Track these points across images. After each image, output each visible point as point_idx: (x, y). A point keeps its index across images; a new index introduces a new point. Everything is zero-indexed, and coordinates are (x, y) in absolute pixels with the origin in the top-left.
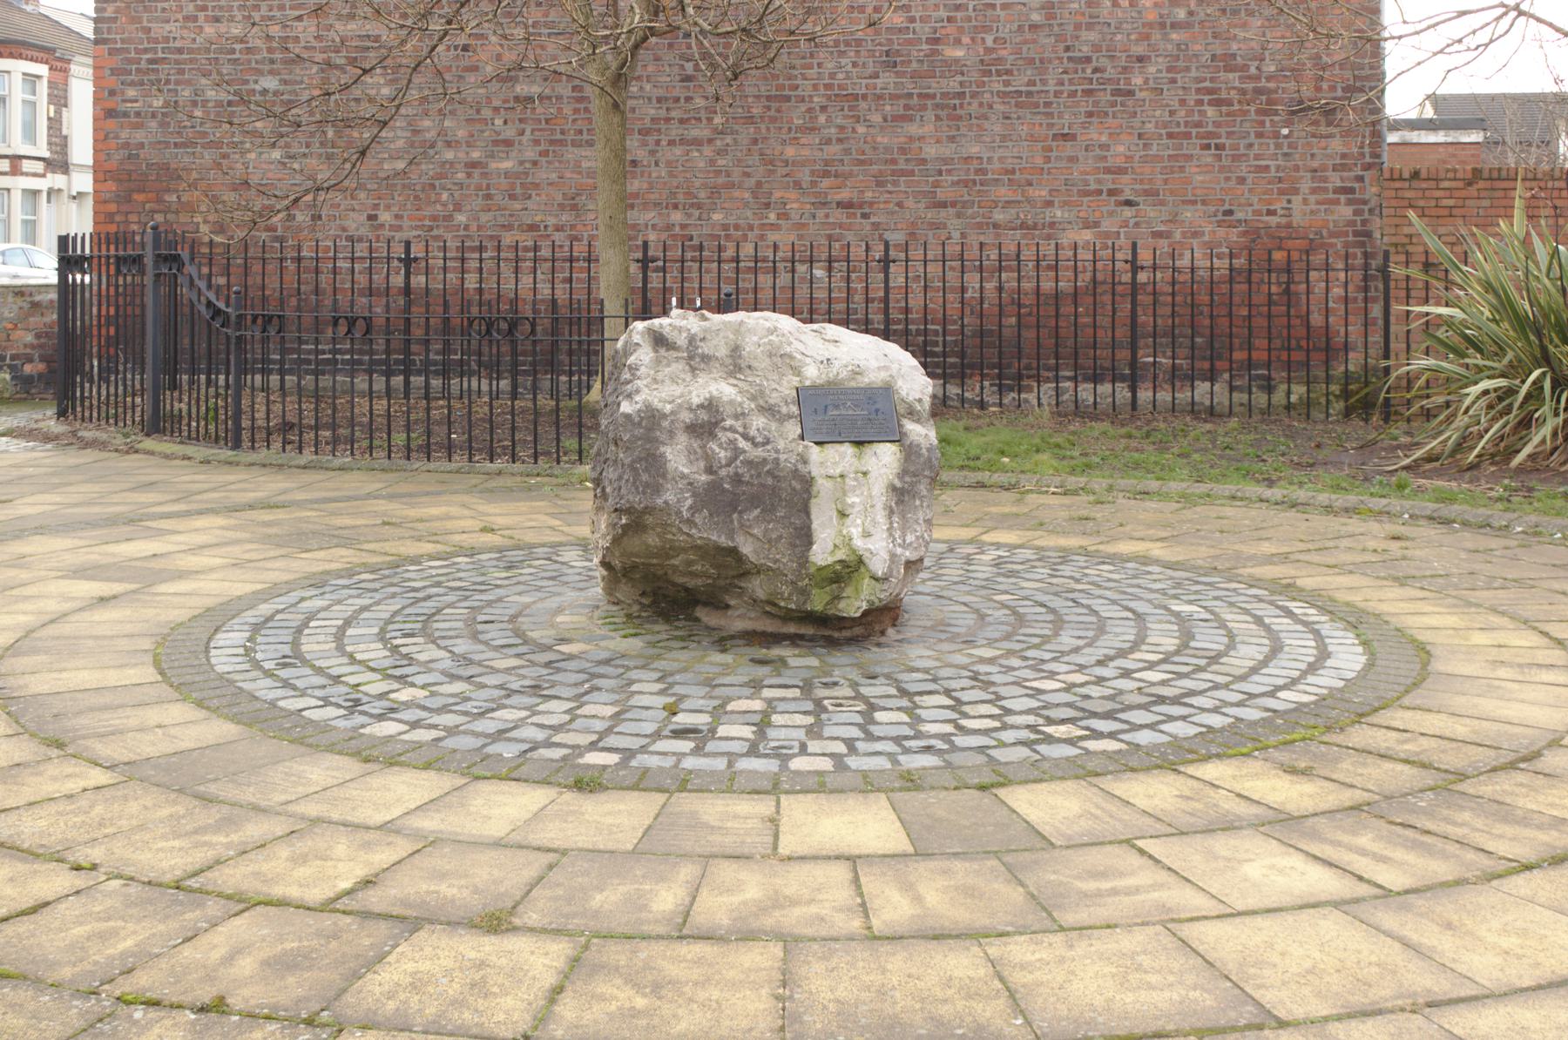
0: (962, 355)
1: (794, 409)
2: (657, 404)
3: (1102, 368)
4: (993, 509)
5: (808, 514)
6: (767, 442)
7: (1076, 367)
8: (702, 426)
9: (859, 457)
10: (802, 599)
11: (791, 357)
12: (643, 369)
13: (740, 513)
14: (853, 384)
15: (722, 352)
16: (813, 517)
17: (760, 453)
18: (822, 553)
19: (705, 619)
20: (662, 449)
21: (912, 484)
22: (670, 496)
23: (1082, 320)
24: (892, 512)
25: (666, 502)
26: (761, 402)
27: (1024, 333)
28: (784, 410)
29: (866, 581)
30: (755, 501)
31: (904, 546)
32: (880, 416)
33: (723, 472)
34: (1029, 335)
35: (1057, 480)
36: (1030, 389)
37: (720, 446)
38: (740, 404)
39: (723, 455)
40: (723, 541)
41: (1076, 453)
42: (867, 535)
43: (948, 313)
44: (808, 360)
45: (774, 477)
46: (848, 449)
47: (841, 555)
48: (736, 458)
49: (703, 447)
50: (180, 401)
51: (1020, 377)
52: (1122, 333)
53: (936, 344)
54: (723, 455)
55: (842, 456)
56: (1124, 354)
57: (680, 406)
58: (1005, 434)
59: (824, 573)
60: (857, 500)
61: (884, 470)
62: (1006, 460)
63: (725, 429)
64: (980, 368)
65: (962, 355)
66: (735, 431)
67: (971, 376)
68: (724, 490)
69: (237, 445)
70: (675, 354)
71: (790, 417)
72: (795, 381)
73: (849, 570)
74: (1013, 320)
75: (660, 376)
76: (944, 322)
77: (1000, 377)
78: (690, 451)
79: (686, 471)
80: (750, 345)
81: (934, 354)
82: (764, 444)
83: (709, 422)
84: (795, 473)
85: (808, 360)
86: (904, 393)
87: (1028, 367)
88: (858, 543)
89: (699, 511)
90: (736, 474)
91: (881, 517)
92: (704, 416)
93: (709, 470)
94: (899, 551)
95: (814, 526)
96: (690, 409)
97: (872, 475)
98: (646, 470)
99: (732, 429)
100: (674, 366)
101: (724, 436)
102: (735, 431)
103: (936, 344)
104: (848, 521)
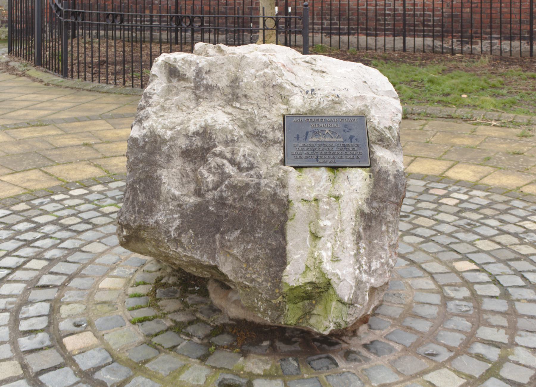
0: (442, 26)
1: (279, 135)
2: (160, 130)
3: (514, 33)
4: (457, 141)
5: (284, 236)
6: (251, 167)
7: (501, 33)
8: (195, 152)
9: (333, 181)
10: (276, 314)
11: (281, 87)
12: (155, 98)
13: (222, 233)
14: (332, 112)
15: (224, 83)
16: (288, 238)
17: (242, 178)
18: (294, 275)
19: (212, 296)
20: (159, 172)
21: (380, 210)
22: (160, 217)
23: (505, 10)
24: (359, 238)
25: (157, 222)
26: (250, 129)
27: (474, 16)
28: (270, 136)
29: (334, 303)
30: (236, 223)
31: (370, 272)
32: (354, 142)
33: (209, 196)
34: (477, 17)
35: (496, 115)
36: (477, 43)
37: (209, 171)
38: (231, 132)
39: (211, 179)
40: (205, 259)
41: (505, 92)
42: (335, 259)
43: (435, 6)
44: (296, 90)
45: (255, 201)
46: (324, 174)
47: (311, 277)
48: (221, 183)
49: (194, 171)
50: (47, 51)
51: (472, 37)
52: (525, 17)
53: (429, 21)
54: (211, 179)
55: (318, 180)
56: (526, 27)
57: (179, 132)
58: (465, 77)
59: (296, 293)
60: (328, 223)
61: (354, 195)
62: (464, 96)
63: (215, 155)
64: (451, 33)
65: (442, 26)
66: (224, 157)
67: (447, 36)
68: (209, 213)
69: (65, 75)
70: (184, 84)
71: (275, 142)
72: (282, 108)
73: (319, 291)
74: (468, 10)
75: (168, 104)
76: (433, 11)
77: (462, 37)
78: (183, 174)
79: (177, 193)
80: (248, 77)
81: (428, 26)
82: (248, 169)
83: (202, 148)
84: (274, 197)
85: (296, 90)
86: (375, 122)
87: (476, 33)
88: (327, 267)
89: (186, 231)
90: (221, 197)
91: (349, 241)
92: (198, 142)
93: (198, 193)
94: (365, 277)
95: (289, 247)
96: (187, 136)
97: (344, 199)
98: (144, 191)
99: (221, 155)
100: (182, 94)
101: (213, 161)
102: (224, 157)
103: (429, 21)
104: (320, 243)
